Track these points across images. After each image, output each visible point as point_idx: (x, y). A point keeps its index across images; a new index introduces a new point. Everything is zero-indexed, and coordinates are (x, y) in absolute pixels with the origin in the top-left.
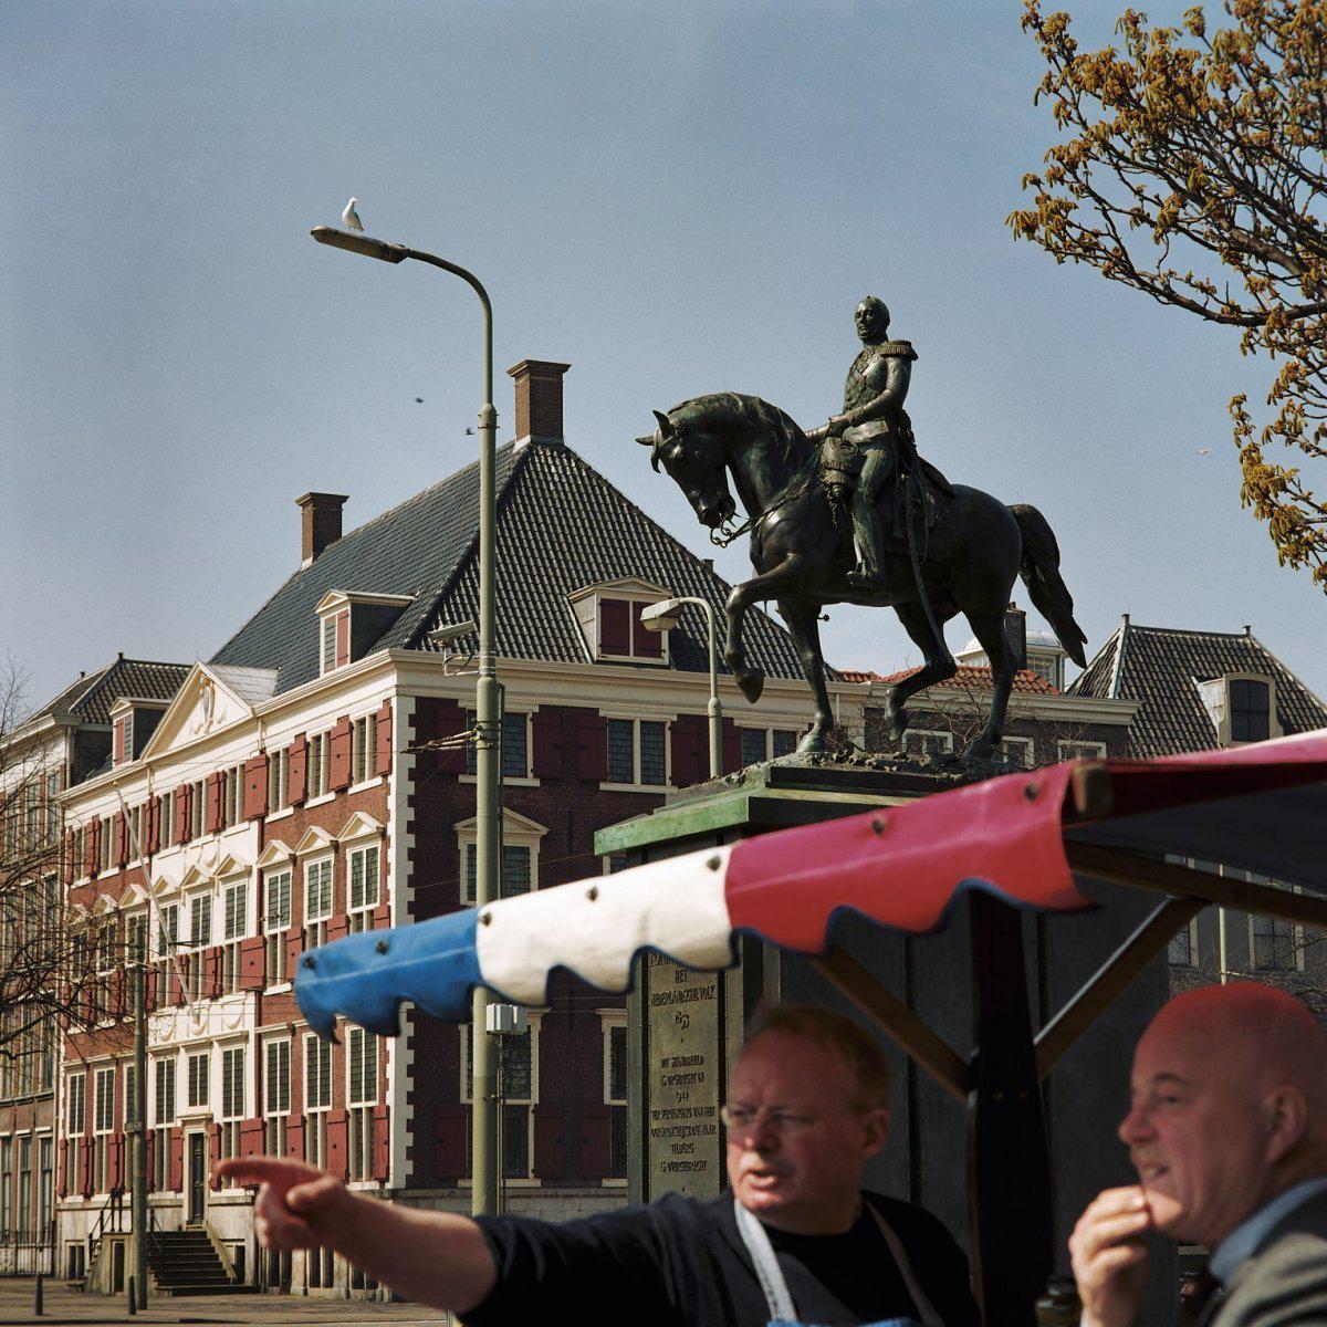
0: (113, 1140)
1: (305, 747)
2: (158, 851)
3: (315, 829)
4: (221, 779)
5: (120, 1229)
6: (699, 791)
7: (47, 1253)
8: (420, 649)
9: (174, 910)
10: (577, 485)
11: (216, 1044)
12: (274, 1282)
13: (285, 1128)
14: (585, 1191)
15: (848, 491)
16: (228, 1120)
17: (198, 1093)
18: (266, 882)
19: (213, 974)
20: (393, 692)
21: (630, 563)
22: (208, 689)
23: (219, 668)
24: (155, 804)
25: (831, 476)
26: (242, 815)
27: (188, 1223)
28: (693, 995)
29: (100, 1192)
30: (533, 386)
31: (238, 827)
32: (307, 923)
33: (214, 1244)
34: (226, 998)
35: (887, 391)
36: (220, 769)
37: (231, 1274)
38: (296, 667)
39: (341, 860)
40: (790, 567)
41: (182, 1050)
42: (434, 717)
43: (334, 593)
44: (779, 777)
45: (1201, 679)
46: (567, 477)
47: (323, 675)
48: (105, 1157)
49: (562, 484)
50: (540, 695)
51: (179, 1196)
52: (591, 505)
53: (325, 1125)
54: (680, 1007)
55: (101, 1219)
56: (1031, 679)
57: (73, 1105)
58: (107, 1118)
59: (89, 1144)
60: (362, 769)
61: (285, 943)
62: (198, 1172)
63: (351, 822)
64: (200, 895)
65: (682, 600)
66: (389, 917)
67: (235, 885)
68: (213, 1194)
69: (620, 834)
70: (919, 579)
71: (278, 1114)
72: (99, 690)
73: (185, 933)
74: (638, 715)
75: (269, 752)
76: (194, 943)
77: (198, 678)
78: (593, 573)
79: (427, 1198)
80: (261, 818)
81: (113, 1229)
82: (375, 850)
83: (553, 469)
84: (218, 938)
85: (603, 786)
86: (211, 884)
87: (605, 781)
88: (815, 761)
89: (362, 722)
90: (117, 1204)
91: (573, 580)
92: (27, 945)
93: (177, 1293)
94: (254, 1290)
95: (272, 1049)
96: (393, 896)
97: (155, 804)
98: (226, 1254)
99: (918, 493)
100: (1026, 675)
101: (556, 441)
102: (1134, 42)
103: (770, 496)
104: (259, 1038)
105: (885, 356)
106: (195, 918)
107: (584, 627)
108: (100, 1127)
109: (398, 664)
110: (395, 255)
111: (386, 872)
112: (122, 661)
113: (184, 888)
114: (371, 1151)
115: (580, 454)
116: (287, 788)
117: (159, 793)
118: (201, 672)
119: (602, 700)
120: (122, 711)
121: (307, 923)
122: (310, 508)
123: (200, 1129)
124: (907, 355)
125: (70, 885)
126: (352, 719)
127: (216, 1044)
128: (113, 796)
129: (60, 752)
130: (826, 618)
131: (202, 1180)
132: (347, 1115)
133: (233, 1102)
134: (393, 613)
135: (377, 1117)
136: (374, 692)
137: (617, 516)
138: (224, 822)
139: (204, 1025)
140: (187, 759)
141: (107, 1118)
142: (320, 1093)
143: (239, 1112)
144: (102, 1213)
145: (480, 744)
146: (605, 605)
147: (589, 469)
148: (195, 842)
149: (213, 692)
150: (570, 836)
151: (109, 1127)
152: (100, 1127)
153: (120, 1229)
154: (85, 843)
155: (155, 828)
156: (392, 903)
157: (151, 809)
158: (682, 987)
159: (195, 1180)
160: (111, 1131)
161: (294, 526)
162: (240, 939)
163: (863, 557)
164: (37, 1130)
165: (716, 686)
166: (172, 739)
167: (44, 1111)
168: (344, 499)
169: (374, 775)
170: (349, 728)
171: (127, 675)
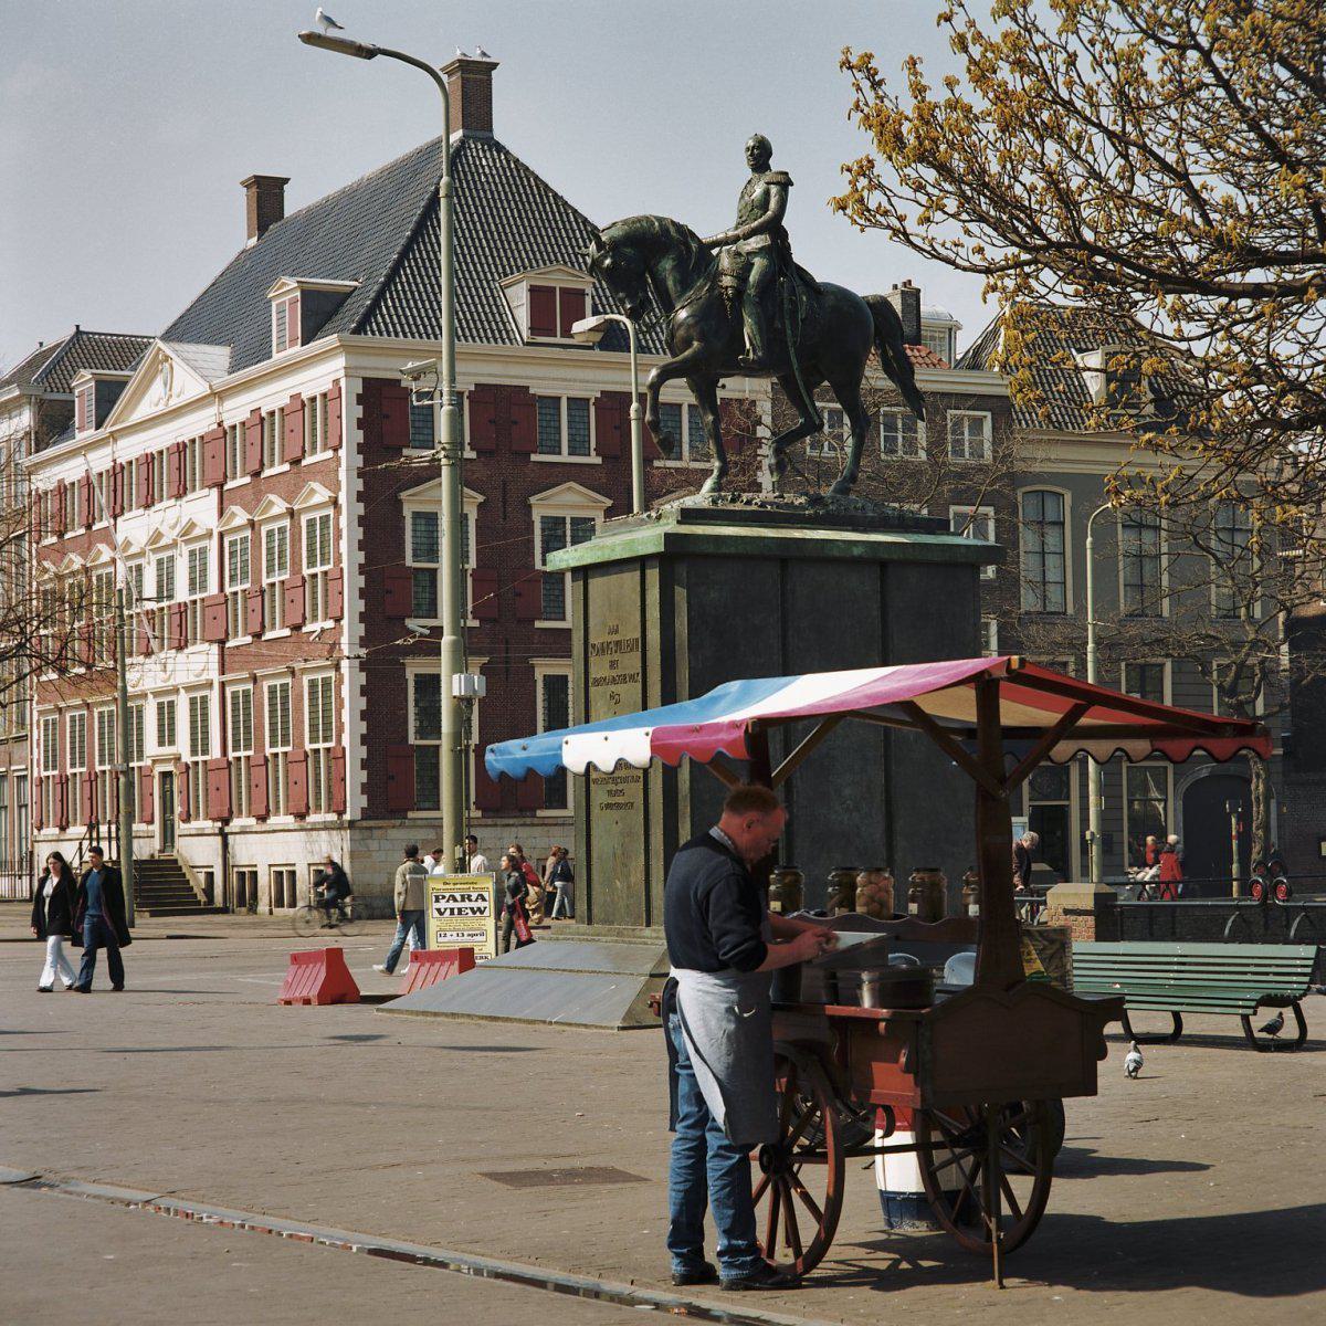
0: (58, 780)
1: (261, 421)
2: (122, 513)
3: (272, 497)
4: (181, 449)
6: (626, 523)
7: (26, 880)
8: (366, 334)
9: (139, 568)
10: (507, 178)
11: (182, 691)
12: (242, 903)
13: (249, 768)
14: (521, 821)
15: (740, 291)
16: (195, 759)
17: (167, 734)
18: (226, 545)
19: (180, 629)
20: (342, 373)
21: (556, 250)
22: (167, 365)
23: (177, 346)
24: (118, 469)
25: (727, 281)
26: (202, 480)
27: (160, 851)
28: (623, 679)
29: (75, 824)
30: (465, 82)
31: (199, 493)
32: (265, 582)
33: (184, 870)
34: (191, 649)
35: (769, 213)
36: (180, 440)
37: (202, 898)
38: (250, 350)
39: (296, 526)
40: (695, 355)
41: (150, 696)
42: (386, 414)
43: (285, 279)
44: (688, 516)
45: (1080, 351)
46: (497, 169)
47: (276, 356)
48: (78, 794)
49: (493, 176)
50: (476, 375)
51: (151, 827)
52: (520, 195)
53: (286, 764)
54: (613, 688)
55: (80, 849)
56: (923, 354)
57: (46, 746)
58: (80, 756)
59: (64, 781)
60: (314, 443)
61: (245, 600)
62: (168, 804)
63: (305, 491)
64: (164, 555)
65: (607, 317)
66: (342, 577)
67: (196, 546)
68: (183, 826)
69: (565, 557)
70: (794, 360)
71: (242, 754)
72: (59, 361)
73: (150, 589)
74: (565, 392)
75: (226, 425)
76: (159, 598)
77: (157, 354)
78: (522, 260)
79: (380, 828)
80: (221, 486)
82: (328, 516)
83: (484, 162)
84: (182, 594)
85: (534, 458)
86: (174, 545)
87: (535, 452)
88: (714, 502)
89: (313, 399)
90: (94, 835)
91: (503, 267)
92: (17, 605)
93: (153, 914)
94: (224, 910)
95: (235, 695)
96: (345, 558)
97: (118, 469)
98: (196, 879)
99: (793, 291)
100: (919, 351)
101: (487, 134)
102: (912, 78)
103: (680, 297)
104: (223, 685)
105: (768, 183)
106: (160, 576)
107: (515, 312)
108: (73, 765)
109: (346, 348)
110: (369, 53)
111: (338, 536)
112: (79, 332)
113: (148, 548)
114: (329, 788)
115: (509, 147)
116: (244, 458)
117: (122, 460)
118: (160, 349)
119: (532, 378)
120: (84, 382)
121: (265, 582)
122: (254, 189)
123: (169, 767)
124: (785, 183)
125: (38, 543)
126: (304, 397)
127: (182, 691)
128: (80, 460)
129: (25, 419)
130: (724, 386)
131: (172, 812)
132: (306, 756)
133: (199, 742)
134: (339, 299)
135: (336, 756)
136: (325, 372)
137: (544, 205)
138: (185, 489)
139: (172, 674)
140: (150, 428)
141: (80, 756)
142: (281, 734)
143: (205, 752)
145: (444, 461)
146: (533, 290)
147: (517, 161)
148: (158, 506)
149: (172, 368)
150: (505, 502)
151: (82, 765)
152: (73, 765)
154: (51, 506)
155: (119, 493)
156: (344, 565)
157: (115, 475)
158: (614, 673)
159: (165, 813)
160: (84, 769)
161: (239, 206)
162: (203, 595)
163: (751, 344)
164: (13, 768)
165: (636, 364)
166: (132, 412)
167: (18, 750)
168: (286, 181)
169: (325, 448)
170: (301, 405)
171: (82, 347)
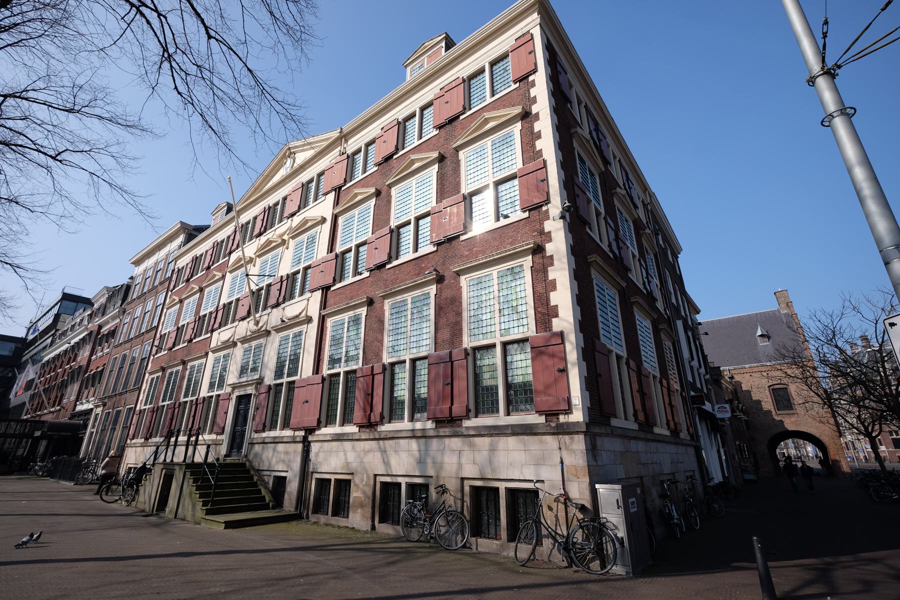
5: (172, 460)
24: (177, 406)
27: (226, 456)
81: (165, 460)
97: (177, 406)
144: (157, 449)
153: (172, 460)
